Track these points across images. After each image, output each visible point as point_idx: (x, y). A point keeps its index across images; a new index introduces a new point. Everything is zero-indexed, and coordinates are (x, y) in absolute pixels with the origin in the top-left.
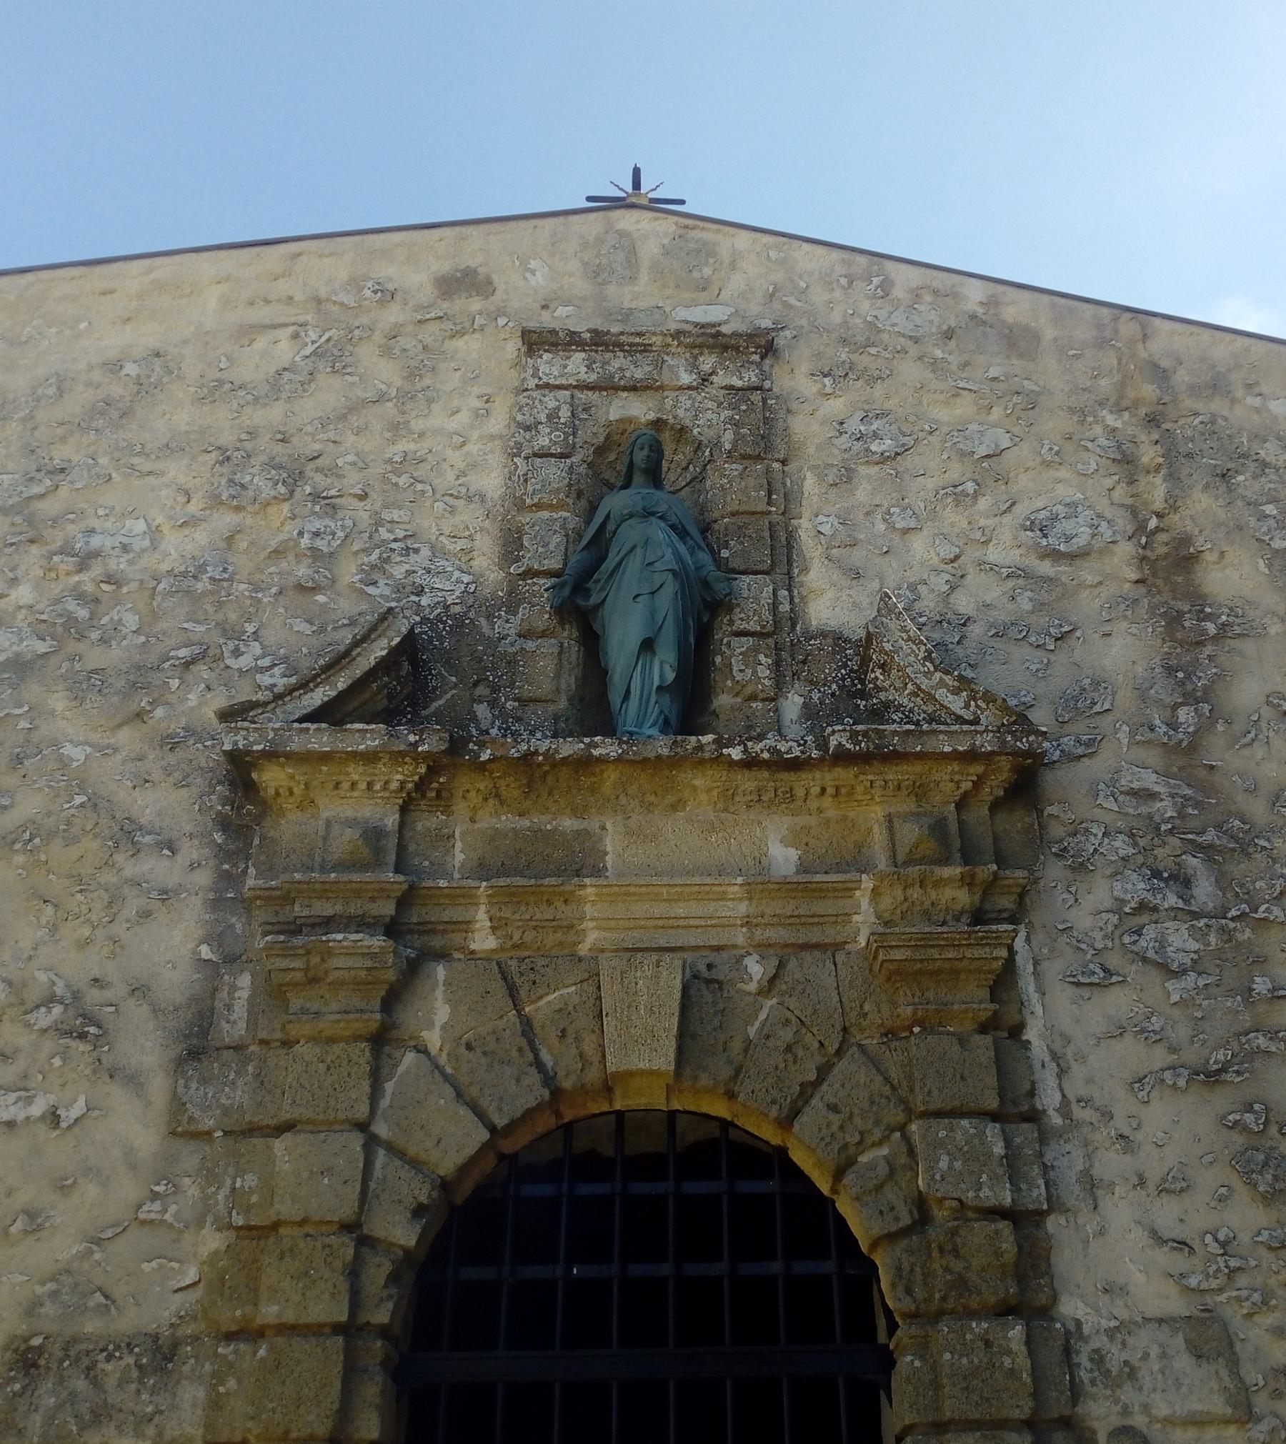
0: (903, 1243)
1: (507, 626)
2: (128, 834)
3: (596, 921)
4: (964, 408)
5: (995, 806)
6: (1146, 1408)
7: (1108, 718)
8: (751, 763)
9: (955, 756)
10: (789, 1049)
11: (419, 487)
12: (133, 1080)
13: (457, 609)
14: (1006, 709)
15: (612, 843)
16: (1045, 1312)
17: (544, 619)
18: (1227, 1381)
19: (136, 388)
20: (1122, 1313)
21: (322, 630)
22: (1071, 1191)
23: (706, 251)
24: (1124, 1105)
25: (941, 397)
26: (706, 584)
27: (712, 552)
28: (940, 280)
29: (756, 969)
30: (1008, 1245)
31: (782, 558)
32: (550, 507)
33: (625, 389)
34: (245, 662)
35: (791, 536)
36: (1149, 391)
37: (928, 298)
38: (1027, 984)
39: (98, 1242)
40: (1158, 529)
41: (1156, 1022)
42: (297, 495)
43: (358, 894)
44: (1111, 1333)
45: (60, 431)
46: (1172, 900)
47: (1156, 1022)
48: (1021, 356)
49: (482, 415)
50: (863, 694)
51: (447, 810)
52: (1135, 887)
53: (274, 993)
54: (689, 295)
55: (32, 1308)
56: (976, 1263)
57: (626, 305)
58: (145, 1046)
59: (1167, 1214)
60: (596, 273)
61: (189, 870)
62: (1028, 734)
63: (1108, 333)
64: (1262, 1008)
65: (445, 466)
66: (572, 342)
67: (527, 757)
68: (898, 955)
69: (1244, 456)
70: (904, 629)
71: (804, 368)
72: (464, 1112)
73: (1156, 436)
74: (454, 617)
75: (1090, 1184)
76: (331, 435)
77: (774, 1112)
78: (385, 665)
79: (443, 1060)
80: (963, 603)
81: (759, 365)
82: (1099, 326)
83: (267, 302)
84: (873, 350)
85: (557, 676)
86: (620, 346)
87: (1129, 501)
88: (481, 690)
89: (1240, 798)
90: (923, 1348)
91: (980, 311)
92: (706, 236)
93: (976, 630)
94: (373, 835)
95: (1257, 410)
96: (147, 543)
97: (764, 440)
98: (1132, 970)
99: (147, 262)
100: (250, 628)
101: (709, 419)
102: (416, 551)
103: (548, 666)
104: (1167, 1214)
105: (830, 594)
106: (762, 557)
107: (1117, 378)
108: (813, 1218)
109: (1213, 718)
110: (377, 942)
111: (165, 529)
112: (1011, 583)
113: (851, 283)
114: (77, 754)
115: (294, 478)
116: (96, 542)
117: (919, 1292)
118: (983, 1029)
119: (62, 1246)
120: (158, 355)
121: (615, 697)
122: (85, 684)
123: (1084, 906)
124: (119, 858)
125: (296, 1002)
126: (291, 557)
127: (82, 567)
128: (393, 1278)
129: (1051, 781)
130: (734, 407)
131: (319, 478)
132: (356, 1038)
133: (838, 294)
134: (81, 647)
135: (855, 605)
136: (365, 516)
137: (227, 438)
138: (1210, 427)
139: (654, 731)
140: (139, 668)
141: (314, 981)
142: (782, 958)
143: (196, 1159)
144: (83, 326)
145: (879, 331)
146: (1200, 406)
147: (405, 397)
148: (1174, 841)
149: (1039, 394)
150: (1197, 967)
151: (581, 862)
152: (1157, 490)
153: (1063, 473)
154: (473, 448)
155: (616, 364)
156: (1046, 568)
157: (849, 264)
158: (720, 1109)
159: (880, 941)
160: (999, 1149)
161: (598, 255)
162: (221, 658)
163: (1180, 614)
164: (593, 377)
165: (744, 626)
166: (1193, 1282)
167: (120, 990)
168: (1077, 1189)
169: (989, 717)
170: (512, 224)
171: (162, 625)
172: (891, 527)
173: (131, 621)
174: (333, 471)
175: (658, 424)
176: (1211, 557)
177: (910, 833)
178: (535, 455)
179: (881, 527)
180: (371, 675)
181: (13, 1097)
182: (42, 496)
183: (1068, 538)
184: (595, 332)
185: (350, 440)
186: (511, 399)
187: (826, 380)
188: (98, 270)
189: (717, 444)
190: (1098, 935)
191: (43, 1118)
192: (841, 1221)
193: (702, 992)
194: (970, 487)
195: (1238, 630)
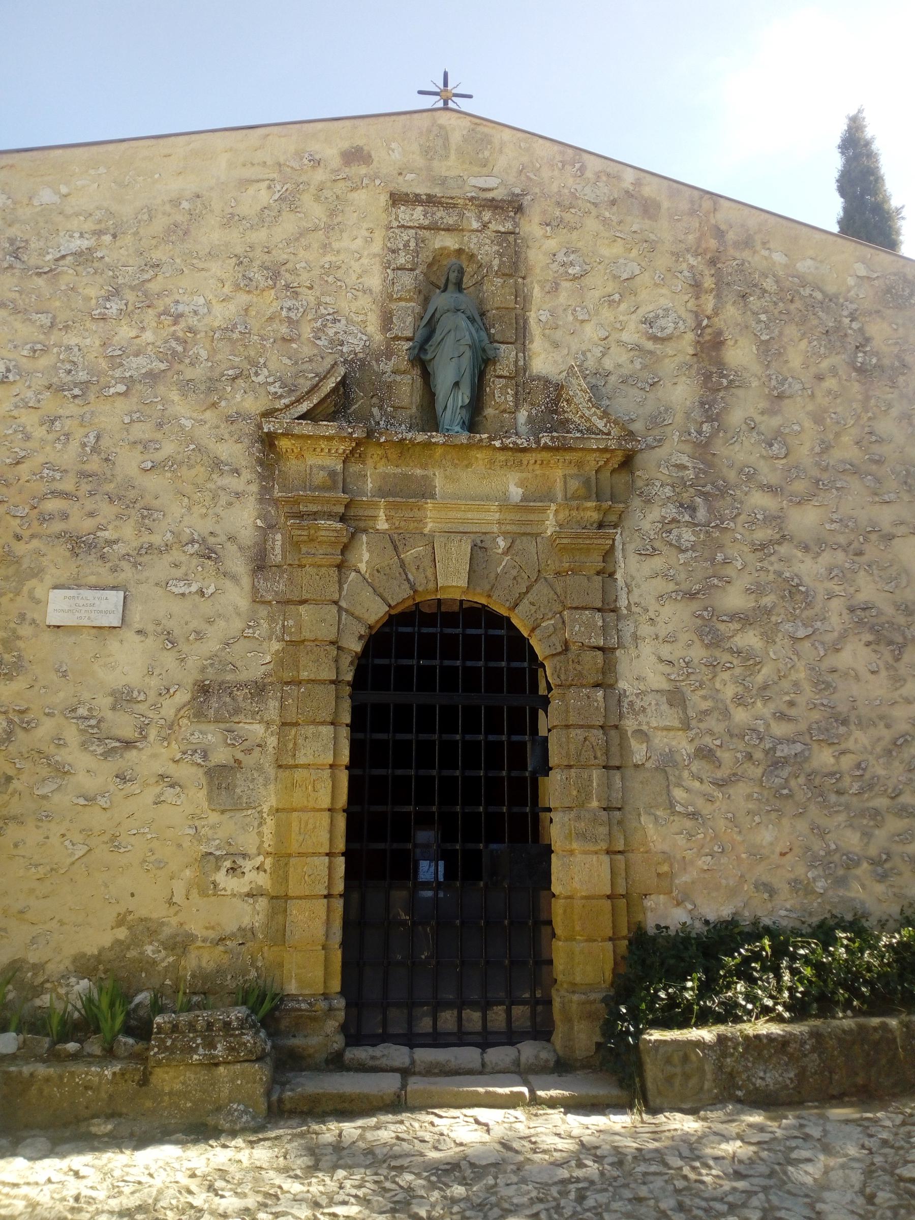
0: (558, 658)
1: (387, 366)
2: (217, 465)
3: (432, 519)
4: (617, 249)
5: (613, 471)
6: (648, 723)
7: (670, 428)
8: (504, 448)
9: (598, 449)
10: (515, 578)
11: (339, 283)
12: (234, 578)
13: (361, 355)
14: (623, 428)
15: (439, 482)
16: (612, 686)
17: (404, 365)
18: (681, 715)
19: (189, 217)
20: (642, 687)
21: (296, 363)
22: (627, 639)
23: (486, 140)
24: (653, 606)
25: (606, 242)
26: (484, 350)
27: (486, 329)
28: (612, 169)
29: (502, 543)
30: (600, 661)
31: (521, 335)
32: (406, 300)
33: (443, 230)
34: (261, 379)
35: (526, 322)
36: (713, 243)
37: (604, 178)
38: (619, 554)
39: (228, 644)
40: (707, 326)
41: (672, 572)
42: (278, 286)
43: (328, 502)
44: (637, 695)
45: (154, 242)
46: (687, 518)
47: (672, 572)
48: (650, 218)
49: (369, 241)
50: (556, 412)
51: (364, 463)
52: (671, 511)
53: (294, 544)
54: (476, 169)
55: (203, 669)
56: (586, 667)
57: (443, 174)
58: (238, 565)
59: (666, 651)
60: (427, 152)
61: (246, 482)
62: (632, 441)
63: (696, 207)
64: (718, 567)
65: (351, 271)
66: (417, 200)
67: (402, 440)
68: (565, 541)
69: (755, 286)
70: (579, 385)
71: (536, 219)
72: (377, 598)
73: (713, 272)
74: (360, 360)
75: (636, 637)
76: (291, 250)
77: (508, 604)
78: (334, 390)
79: (367, 576)
80: (608, 364)
81: (513, 218)
82: (692, 202)
83: (253, 165)
84: (573, 211)
85: (411, 395)
86: (441, 203)
87: (695, 309)
88: (375, 400)
89: (725, 470)
90: (563, 697)
91: (631, 188)
92: (486, 130)
93: (612, 379)
94: (332, 474)
95: (766, 258)
96: (206, 310)
97: (514, 265)
98: (665, 549)
99: (187, 137)
100: (262, 361)
101: (486, 250)
102: (339, 321)
103: (407, 389)
104: (666, 651)
105: (543, 356)
106: (510, 335)
107: (698, 235)
108: (519, 646)
109: (718, 430)
110: (339, 525)
111: (214, 302)
112: (632, 353)
113: (563, 166)
114: (188, 424)
115: (276, 275)
116: (181, 308)
117: (563, 677)
118: (598, 573)
119: (212, 645)
120: (198, 197)
121: (439, 408)
122: (186, 387)
123: (647, 519)
124: (214, 476)
125: (304, 549)
126: (277, 321)
127: (175, 323)
128: (352, 663)
129: (639, 459)
130: (500, 244)
131: (287, 275)
132: (331, 566)
133: (556, 173)
134: (181, 367)
135: (555, 362)
136: (312, 299)
137: (239, 250)
138: (741, 268)
139: (458, 428)
140: (210, 380)
141: (312, 540)
142: (513, 539)
143: (265, 612)
144: (157, 176)
145: (577, 198)
146: (737, 255)
147: (329, 228)
148: (692, 490)
149: (657, 242)
150: (693, 548)
151: (425, 492)
152: (709, 303)
153: (664, 291)
154: (365, 261)
155: (439, 214)
156: (650, 345)
157: (562, 153)
158: (483, 601)
159: (558, 535)
160: (600, 623)
161: (428, 140)
162: (249, 376)
163: (712, 373)
164: (427, 222)
165: (501, 373)
166: (672, 677)
167: (222, 538)
168: (629, 639)
169: (615, 432)
170: (381, 119)
171: (219, 357)
172: (576, 318)
173: (204, 354)
174: (294, 271)
175: (460, 251)
176: (730, 343)
177: (574, 485)
178: (398, 269)
179: (571, 318)
180: (328, 396)
181: (182, 583)
182: (150, 280)
183: (663, 329)
184: (428, 195)
185: (302, 253)
186: (384, 232)
187: (548, 228)
188: (161, 141)
189: (490, 267)
190: (652, 533)
191: (196, 592)
192: (531, 648)
193: (480, 550)
194: (617, 297)
195: (737, 384)
